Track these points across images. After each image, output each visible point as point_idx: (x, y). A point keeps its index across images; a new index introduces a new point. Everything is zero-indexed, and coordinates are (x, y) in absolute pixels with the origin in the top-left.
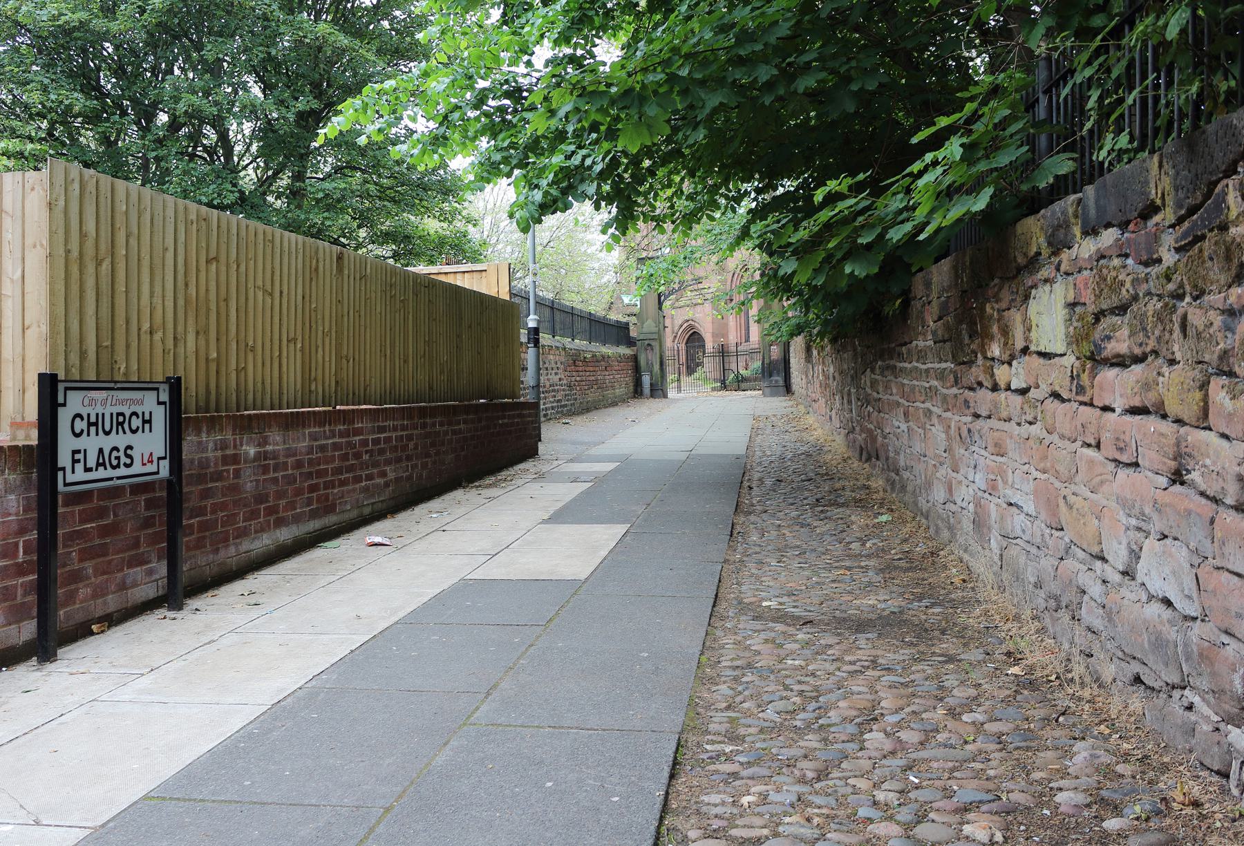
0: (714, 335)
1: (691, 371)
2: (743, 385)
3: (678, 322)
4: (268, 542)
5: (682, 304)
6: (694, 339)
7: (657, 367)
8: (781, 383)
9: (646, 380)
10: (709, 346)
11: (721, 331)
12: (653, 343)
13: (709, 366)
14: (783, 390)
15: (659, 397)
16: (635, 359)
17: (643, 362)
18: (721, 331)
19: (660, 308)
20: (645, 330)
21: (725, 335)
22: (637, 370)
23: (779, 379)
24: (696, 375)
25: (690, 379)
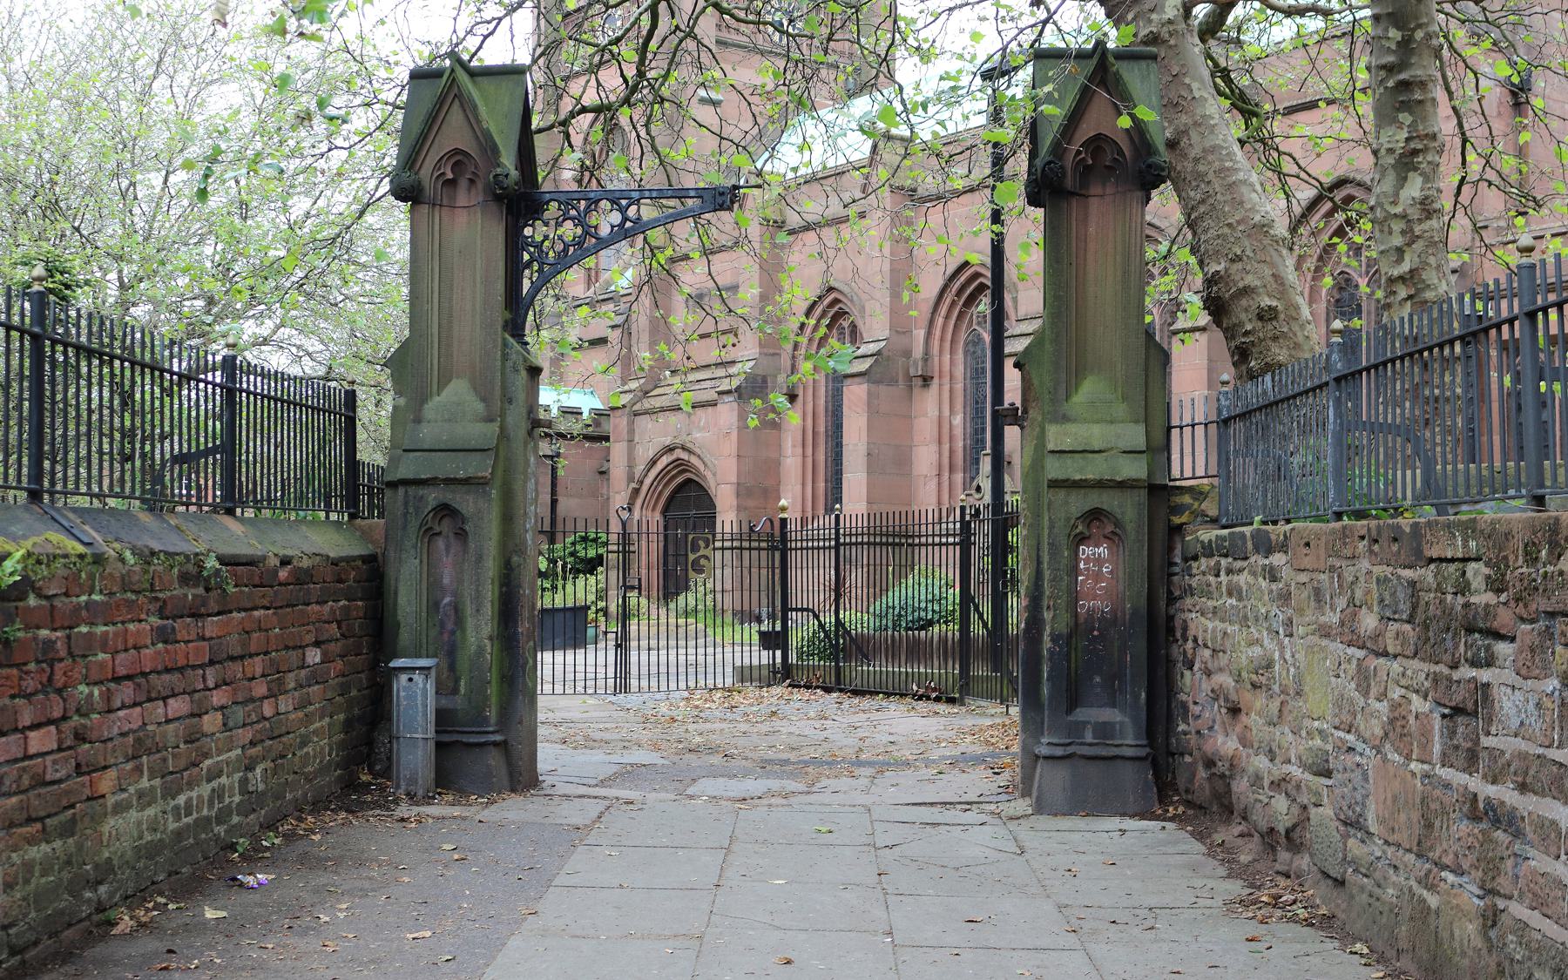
0: (743, 491)
1: (672, 585)
2: (860, 671)
3: (645, 452)
4: (789, 461)
5: (657, 403)
6: (685, 498)
7: (480, 630)
8: (1129, 741)
9: (416, 695)
10: (727, 518)
11: (759, 484)
12: (466, 503)
13: (720, 576)
14: (1133, 778)
15: (488, 788)
16: (370, 579)
17: (407, 601)
18: (759, 484)
19: (515, 328)
20: (428, 433)
21: (770, 492)
22: (375, 637)
23: (1115, 719)
24: (687, 599)
25: (666, 616)
